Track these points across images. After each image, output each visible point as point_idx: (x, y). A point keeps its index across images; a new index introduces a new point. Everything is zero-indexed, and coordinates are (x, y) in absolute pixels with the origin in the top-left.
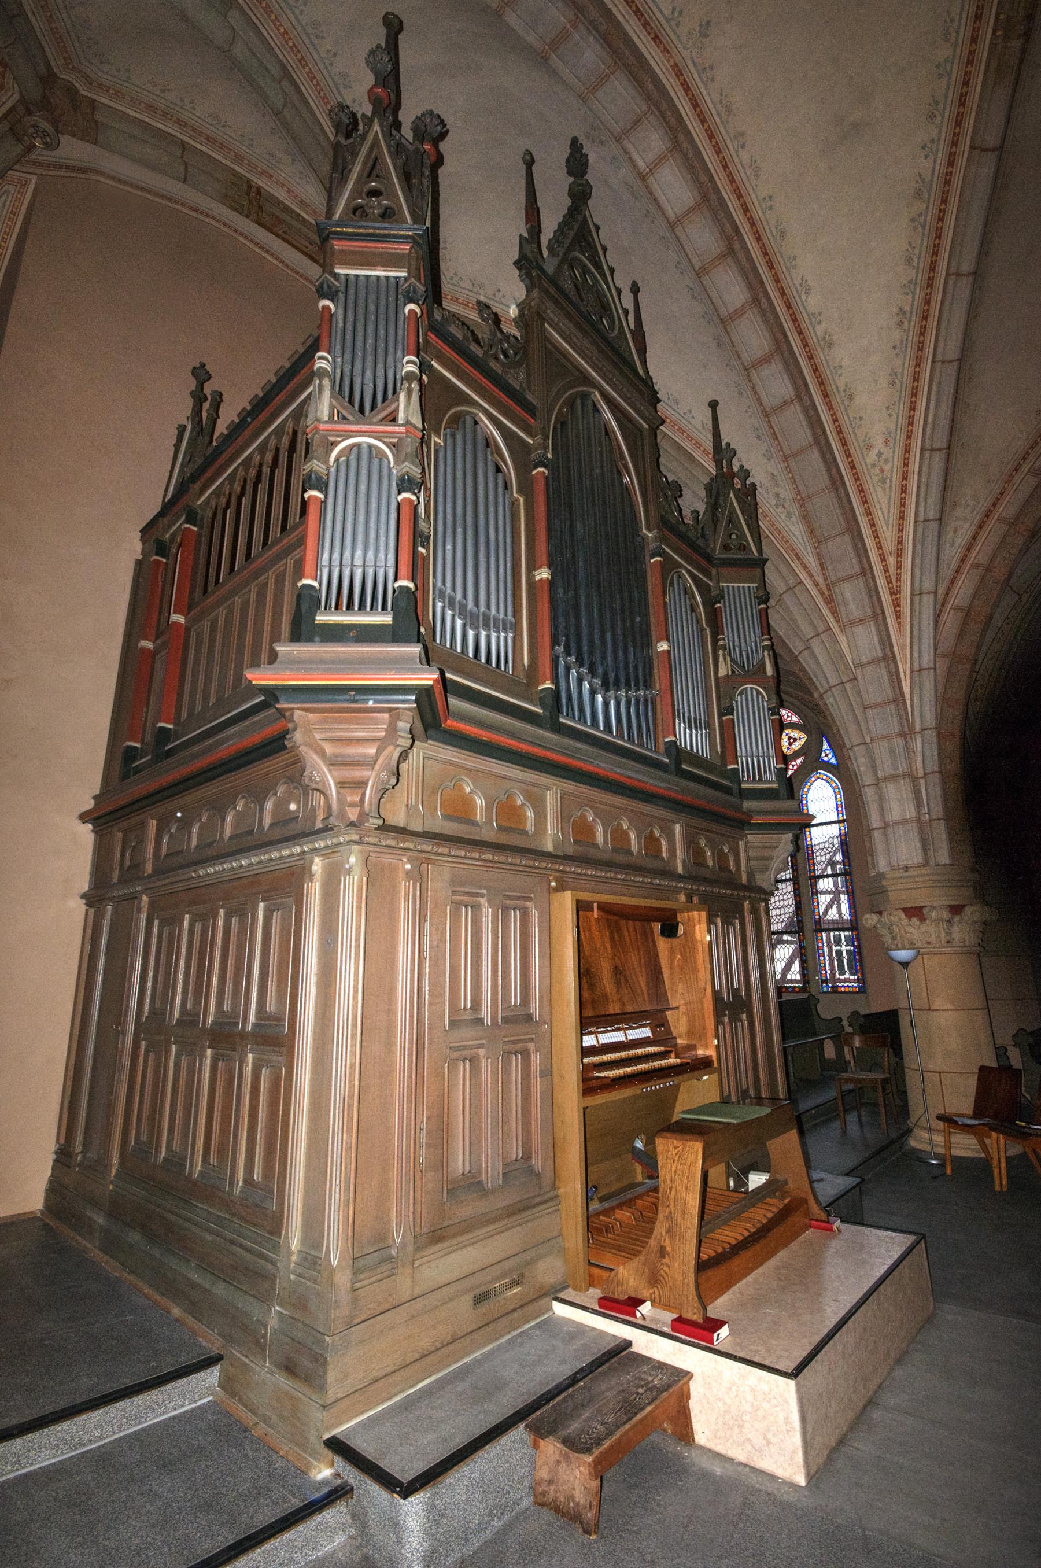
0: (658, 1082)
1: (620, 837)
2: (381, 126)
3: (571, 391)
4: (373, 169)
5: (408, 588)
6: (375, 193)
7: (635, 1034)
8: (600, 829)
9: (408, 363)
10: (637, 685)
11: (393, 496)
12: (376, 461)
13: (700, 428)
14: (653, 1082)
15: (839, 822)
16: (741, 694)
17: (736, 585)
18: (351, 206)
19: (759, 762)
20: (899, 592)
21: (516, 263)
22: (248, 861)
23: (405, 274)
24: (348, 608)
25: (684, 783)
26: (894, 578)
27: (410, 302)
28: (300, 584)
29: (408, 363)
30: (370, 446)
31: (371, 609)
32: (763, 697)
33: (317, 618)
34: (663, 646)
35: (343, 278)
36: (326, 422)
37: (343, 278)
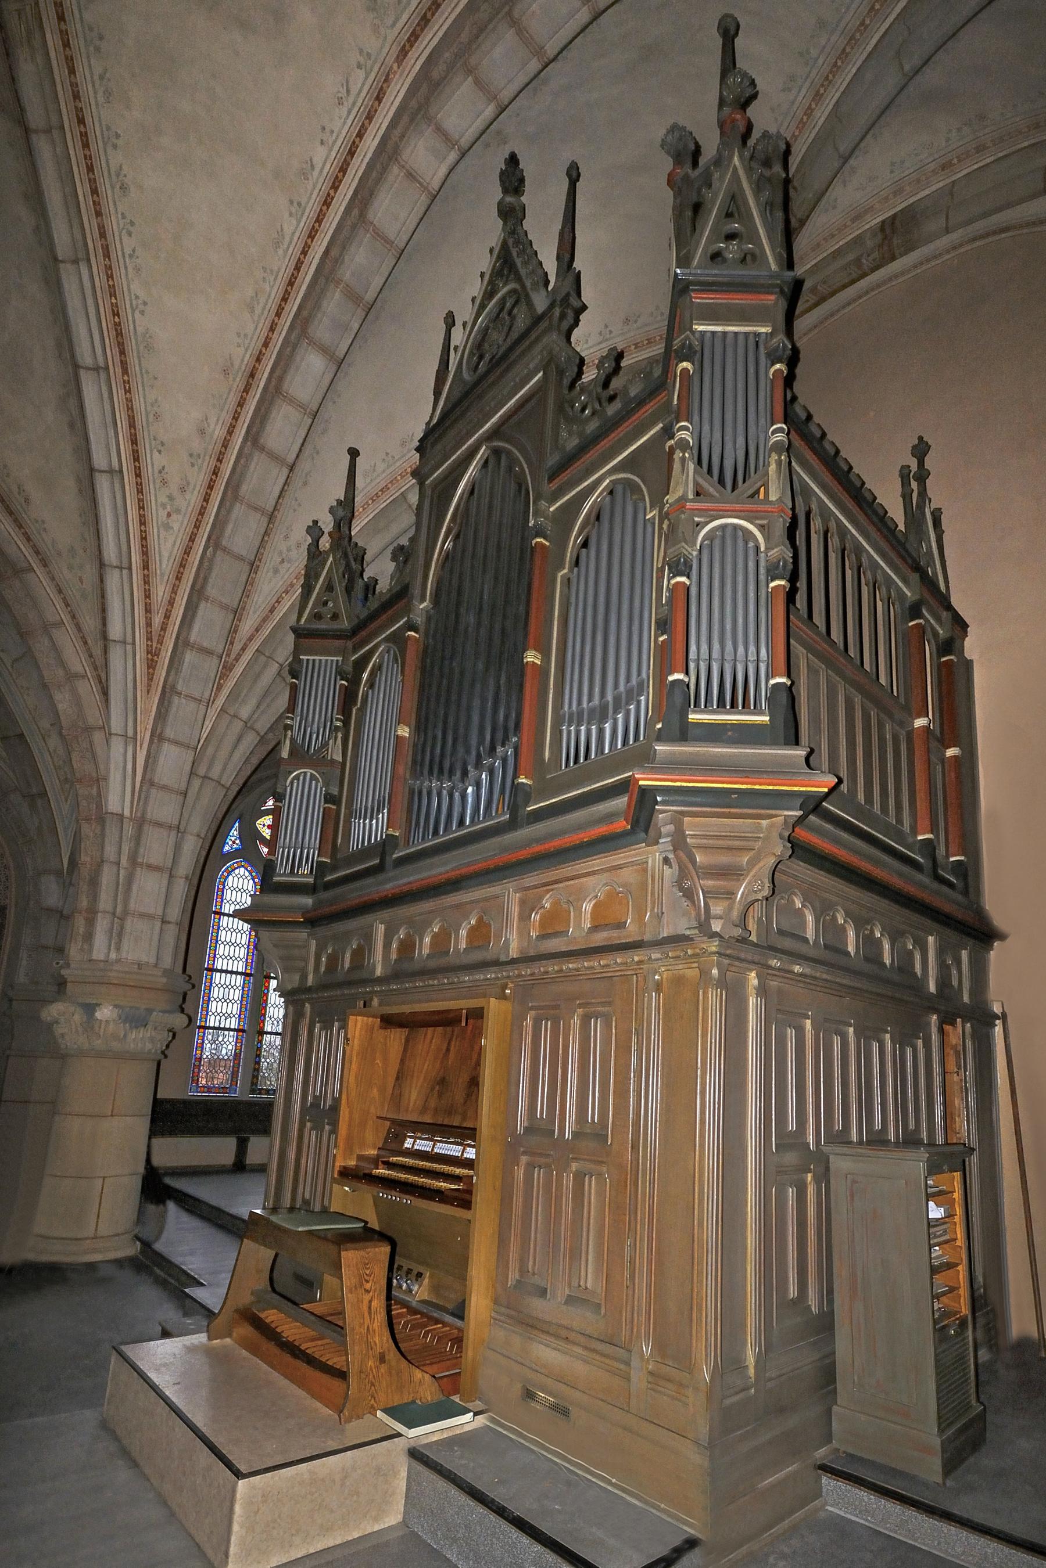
0: (397, 1194)
1: (869, 944)
2: (741, 157)
3: (509, 447)
4: (733, 209)
5: (682, 681)
6: (730, 237)
7: (423, 1145)
8: (851, 934)
9: (773, 433)
10: (431, 773)
11: (763, 583)
12: (740, 543)
13: (156, 471)
14: (393, 1193)
15: (220, 914)
16: (297, 777)
17: (323, 658)
18: (710, 251)
19: (289, 852)
20: (158, 655)
21: (584, 308)
22: (529, 971)
23: (769, 330)
24: (732, 707)
25: (936, 885)
26: (155, 639)
27: (682, 361)
28: (671, 678)
29: (773, 433)
30: (735, 527)
31: (743, 707)
32: (317, 781)
33: (690, 716)
34: (404, 732)
35: (697, 335)
36: (692, 501)
37: (697, 335)
